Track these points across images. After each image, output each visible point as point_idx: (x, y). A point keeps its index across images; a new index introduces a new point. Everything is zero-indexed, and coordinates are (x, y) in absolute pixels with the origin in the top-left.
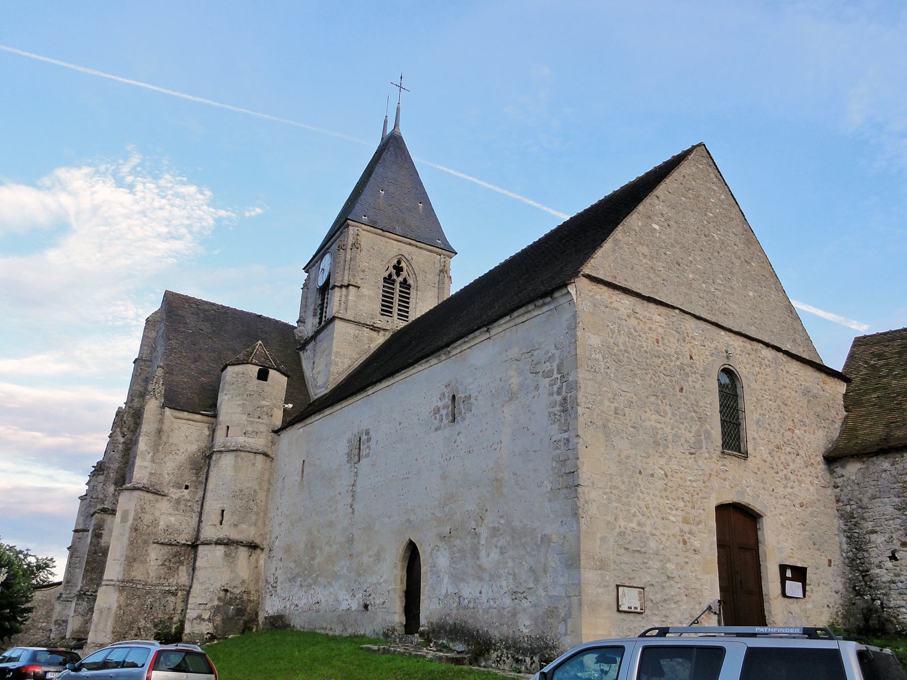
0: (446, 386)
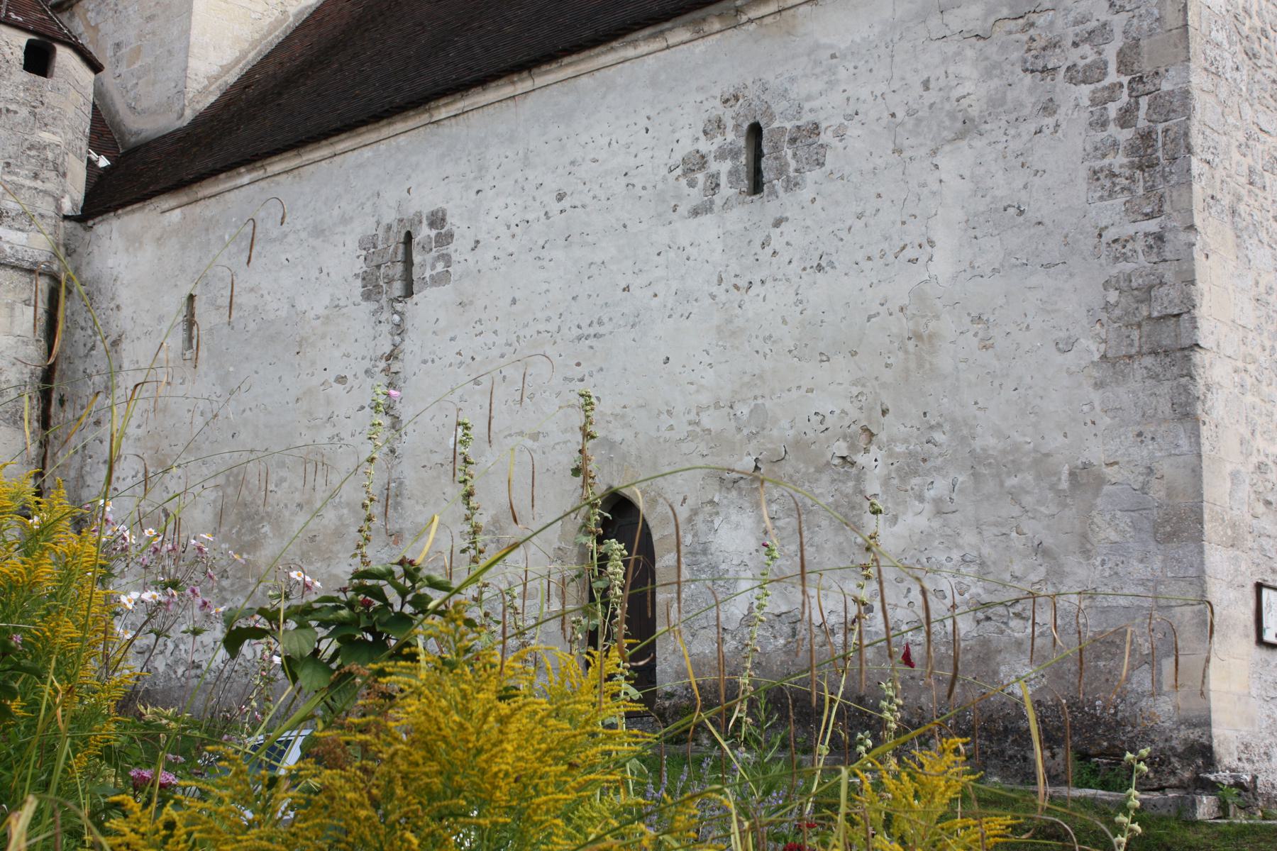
0: (727, 100)
